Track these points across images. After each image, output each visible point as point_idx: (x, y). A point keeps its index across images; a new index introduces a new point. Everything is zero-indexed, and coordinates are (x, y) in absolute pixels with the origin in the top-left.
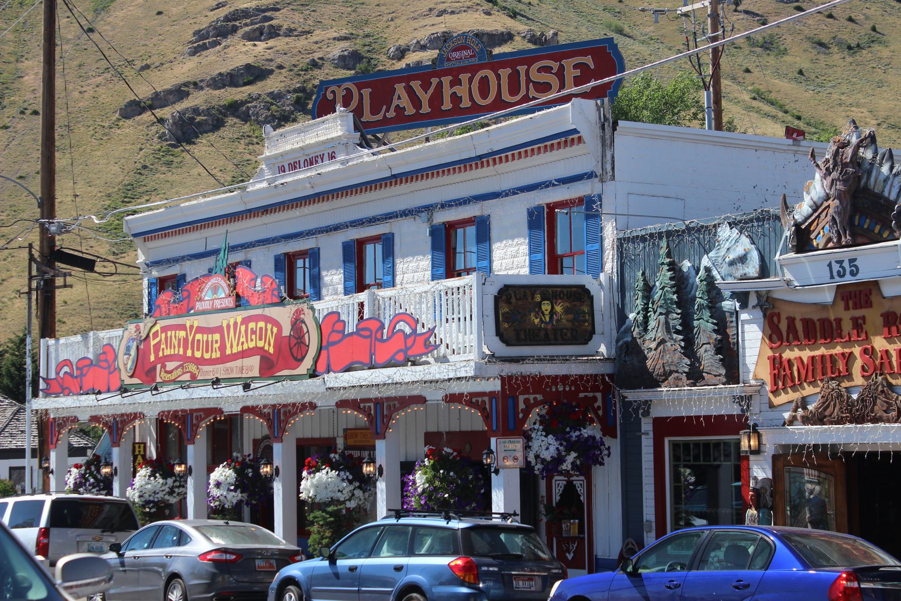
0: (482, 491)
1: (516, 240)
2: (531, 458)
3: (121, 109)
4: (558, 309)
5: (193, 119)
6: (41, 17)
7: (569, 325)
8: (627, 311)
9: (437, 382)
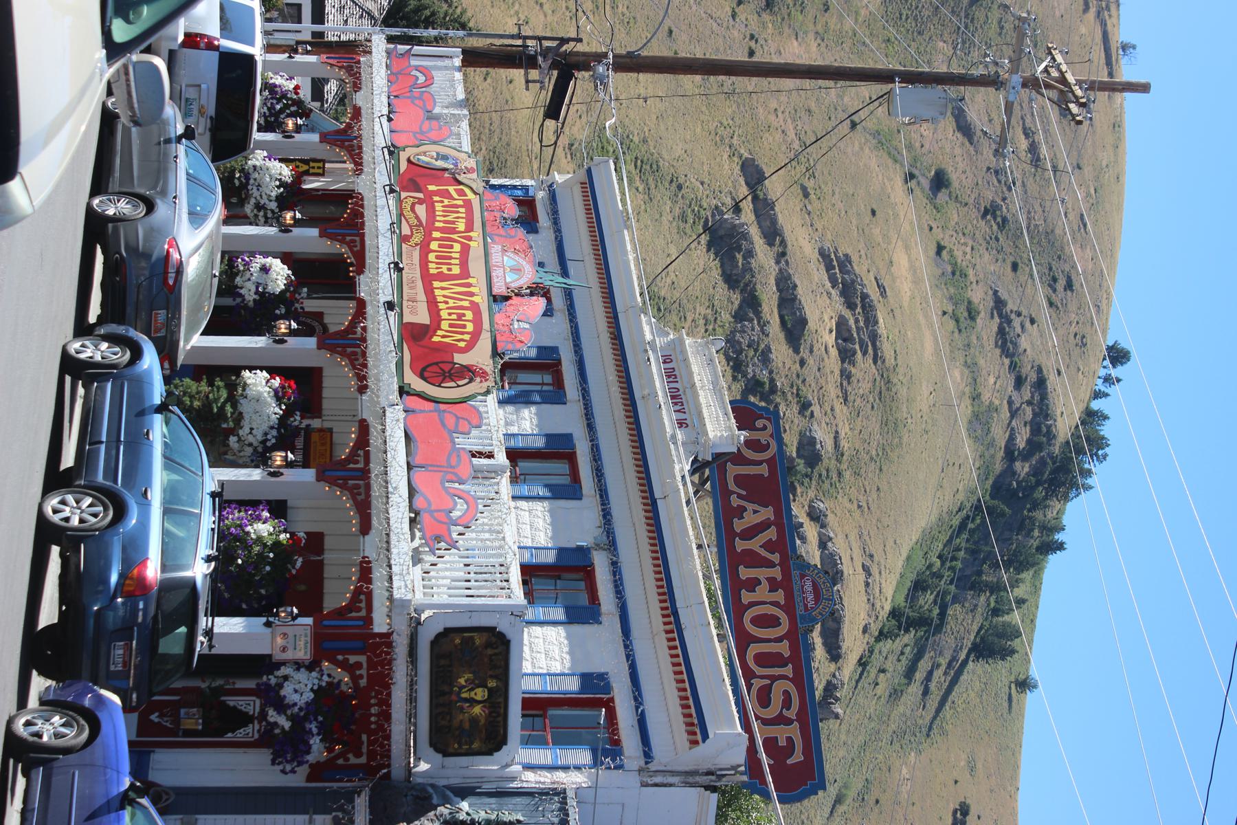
0: (244, 606)
1: (568, 657)
2: (284, 671)
3: (753, 160)
4: (477, 710)
5: (739, 249)
6: (870, 64)
7: (456, 723)
8: (473, 799)
9: (388, 550)
